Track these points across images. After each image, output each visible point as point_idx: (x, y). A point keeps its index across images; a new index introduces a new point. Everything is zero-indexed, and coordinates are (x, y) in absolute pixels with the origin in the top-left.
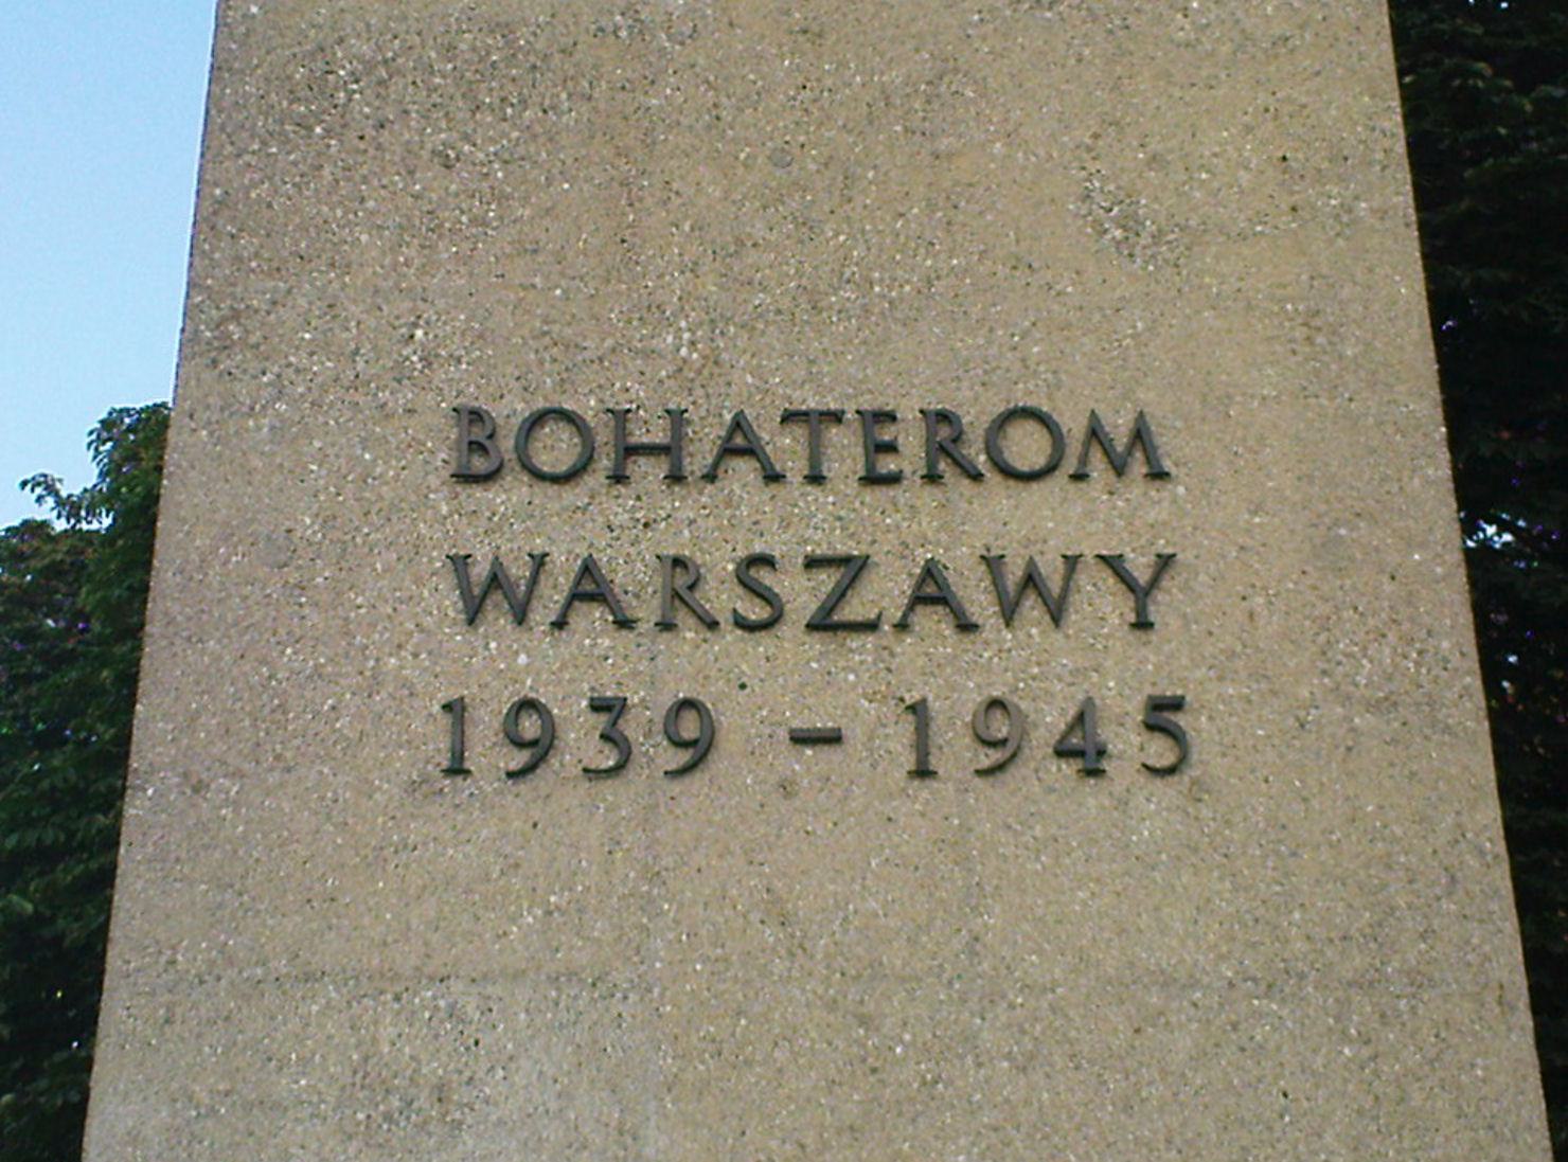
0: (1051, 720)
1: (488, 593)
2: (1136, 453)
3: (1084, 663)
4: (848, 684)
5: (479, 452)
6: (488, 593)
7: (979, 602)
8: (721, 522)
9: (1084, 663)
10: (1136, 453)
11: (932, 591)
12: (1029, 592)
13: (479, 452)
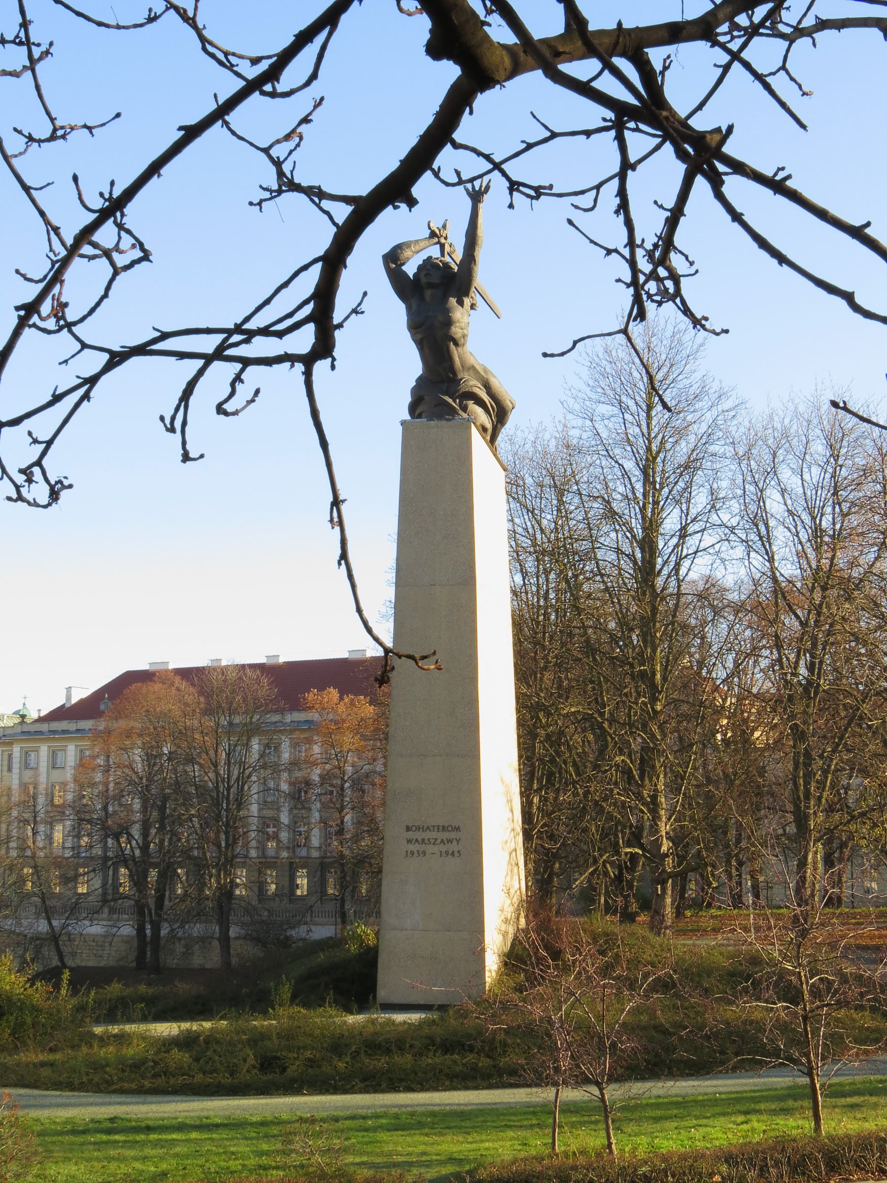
2: (458, 829)
3: (453, 847)
4: (436, 849)
6: (409, 841)
8: (428, 835)
9: (453, 847)
10: (458, 829)
11: (442, 841)
12: (450, 841)
13: (408, 829)
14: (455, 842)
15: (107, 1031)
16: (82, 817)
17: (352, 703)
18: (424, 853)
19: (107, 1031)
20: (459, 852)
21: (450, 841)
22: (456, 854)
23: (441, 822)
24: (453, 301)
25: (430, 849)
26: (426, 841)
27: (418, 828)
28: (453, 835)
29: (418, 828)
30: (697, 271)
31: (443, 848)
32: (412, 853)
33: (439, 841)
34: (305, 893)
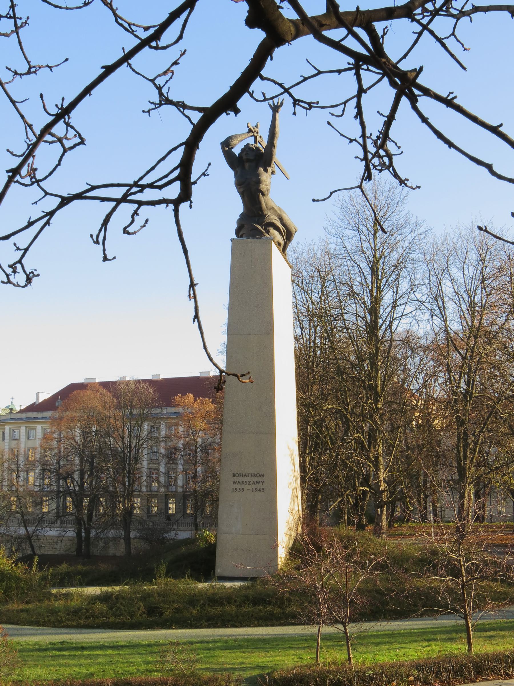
0: (258, 489)
2: (263, 476)
4: (250, 487)
5: (234, 475)
6: (234, 483)
8: (245, 479)
10: (263, 476)
11: (254, 482)
12: (258, 483)
13: (234, 475)
18: (243, 489)
20: (263, 489)
21: (258, 483)
23: (252, 471)
24: (261, 169)
25: (246, 487)
26: (244, 483)
27: (240, 475)
28: (260, 479)
29: (240, 475)
31: (254, 487)
32: (236, 489)
33: (252, 483)
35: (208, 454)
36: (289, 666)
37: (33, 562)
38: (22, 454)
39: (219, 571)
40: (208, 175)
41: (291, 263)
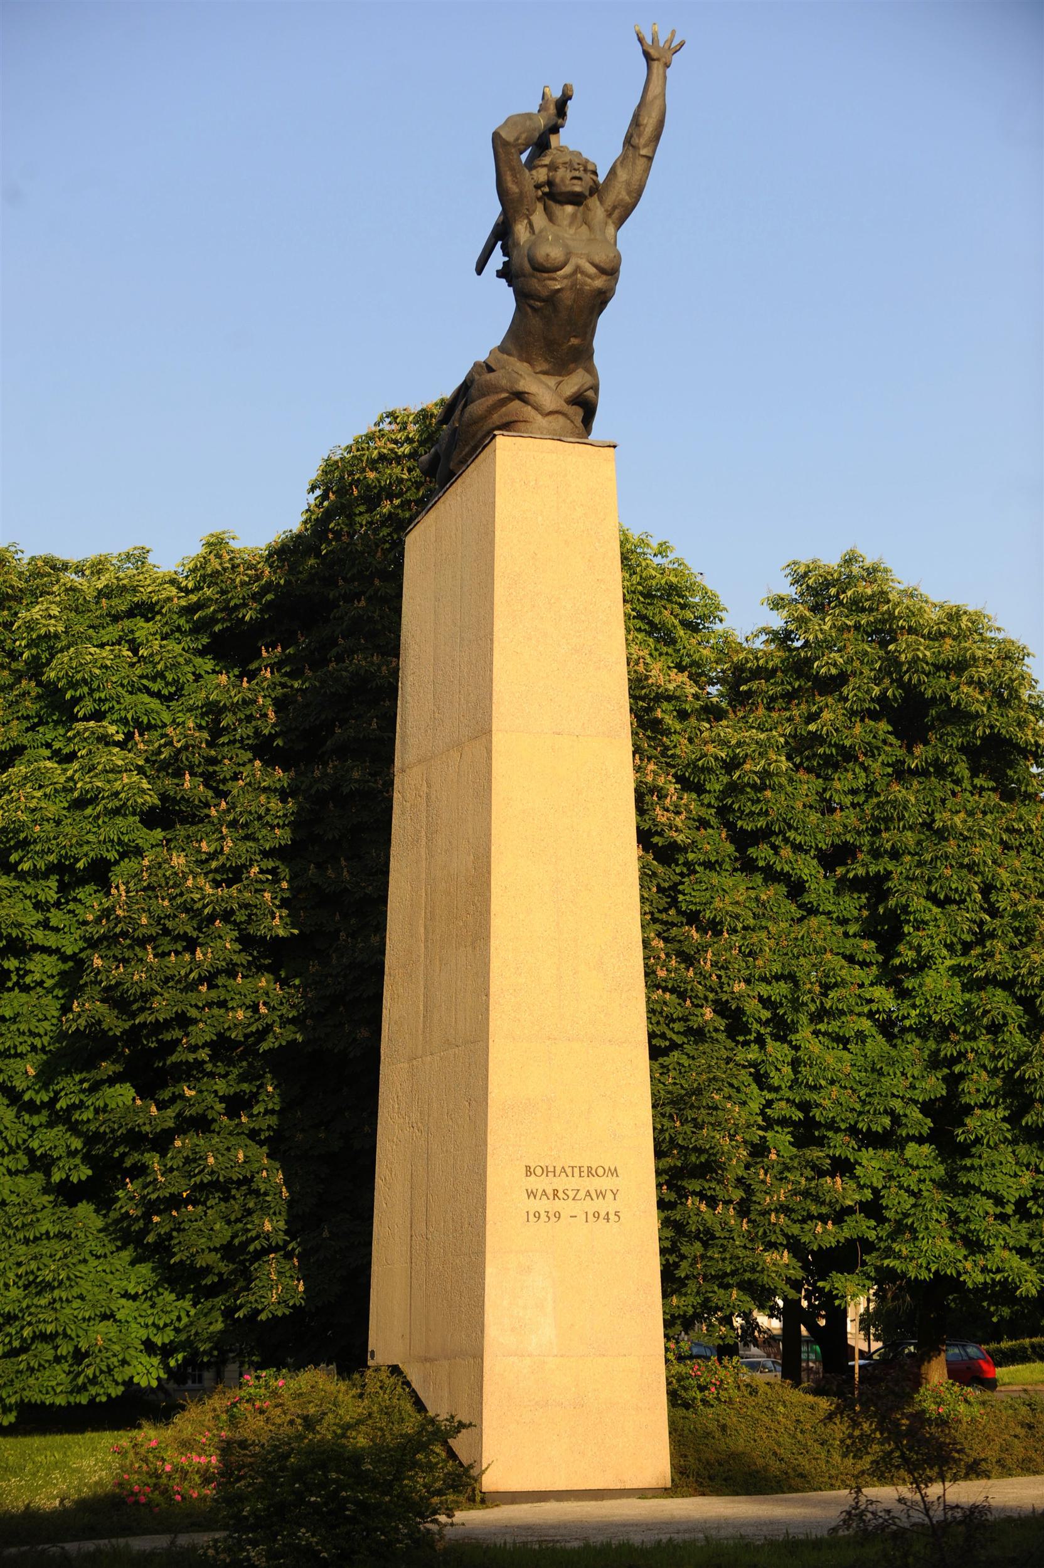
1: (531, 1194)
2: (614, 1172)
5: (529, 1171)
6: (531, 1194)
7: (594, 1196)
8: (561, 1183)
10: (614, 1172)
12: (601, 1194)
13: (529, 1171)
14: (610, 1196)
15: (919, 1483)
16: (521, 193)
17: (111, 1029)
18: (558, 1216)
19: (919, 1483)
20: (616, 1214)
21: (601, 1194)
22: (612, 1216)
25: (565, 1207)
26: (561, 1194)
27: (545, 1171)
29: (545, 1171)
30: (480, 270)
31: (591, 1206)
33: (582, 1194)
34: (932, 1125)
35: (681, 668)
36: (165, 1545)
37: (52, 1405)
38: (173, 1543)
39: (490, 1482)
40: (682, 45)
41: (650, 95)
